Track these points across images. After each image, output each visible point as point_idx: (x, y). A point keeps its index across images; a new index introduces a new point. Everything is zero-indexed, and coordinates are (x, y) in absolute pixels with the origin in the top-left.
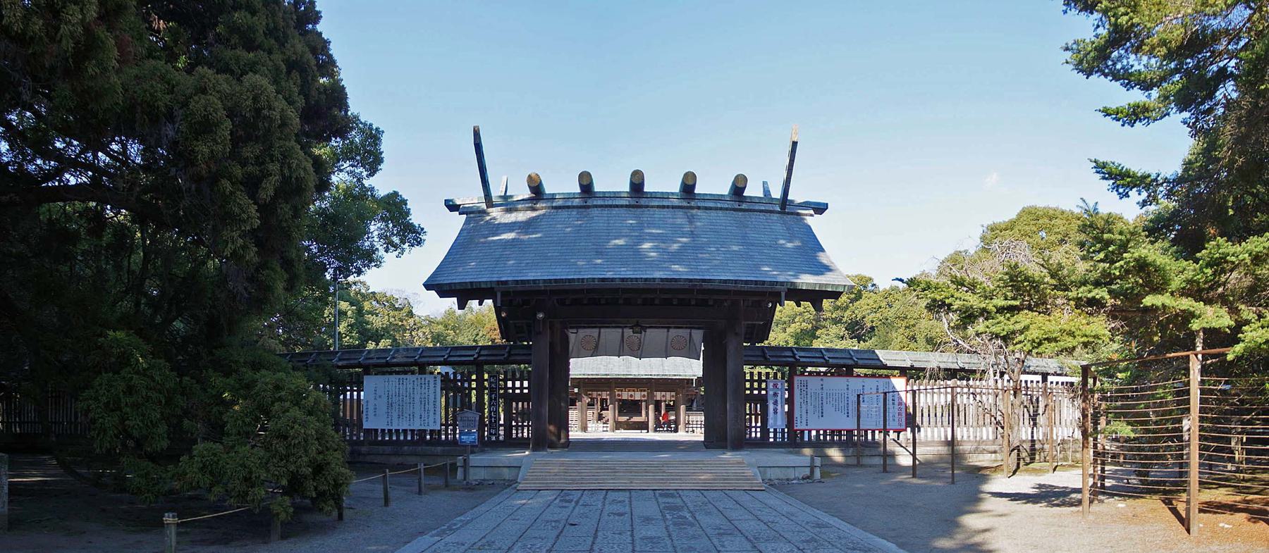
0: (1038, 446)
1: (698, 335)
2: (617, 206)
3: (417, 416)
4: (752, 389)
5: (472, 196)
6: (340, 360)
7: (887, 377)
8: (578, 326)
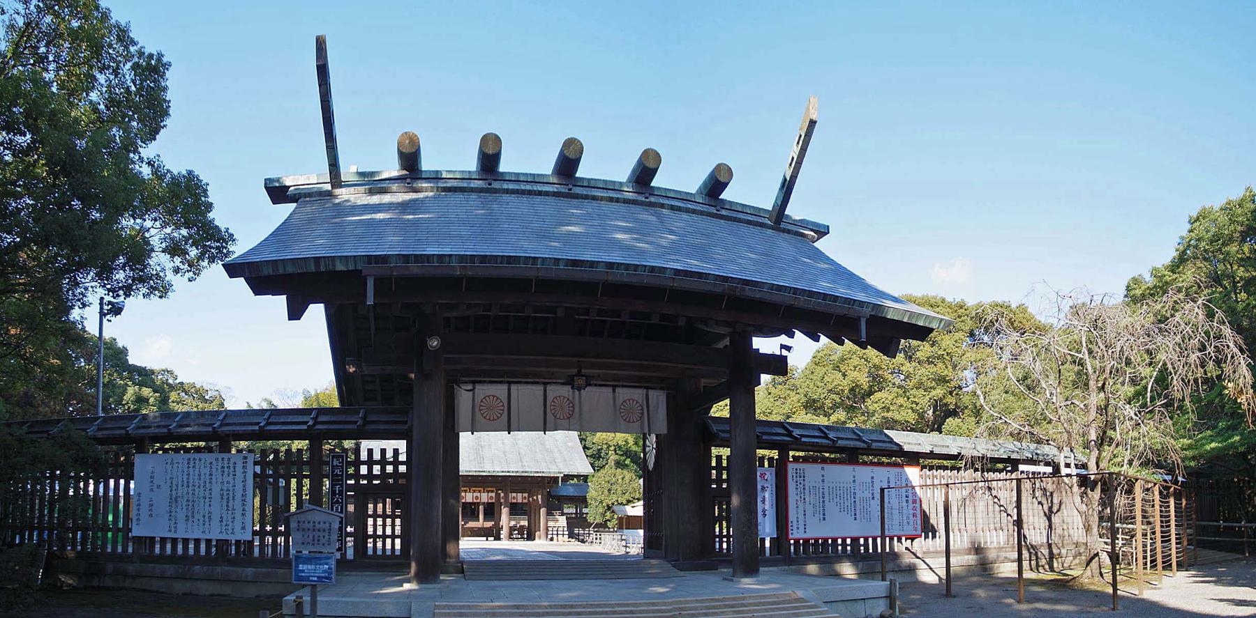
0: (1055, 551)
1: (659, 399)
2: (540, 193)
3: (216, 518)
4: (719, 480)
5: (307, 172)
6: (99, 429)
7: (902, 466)
8: (478, 376)
